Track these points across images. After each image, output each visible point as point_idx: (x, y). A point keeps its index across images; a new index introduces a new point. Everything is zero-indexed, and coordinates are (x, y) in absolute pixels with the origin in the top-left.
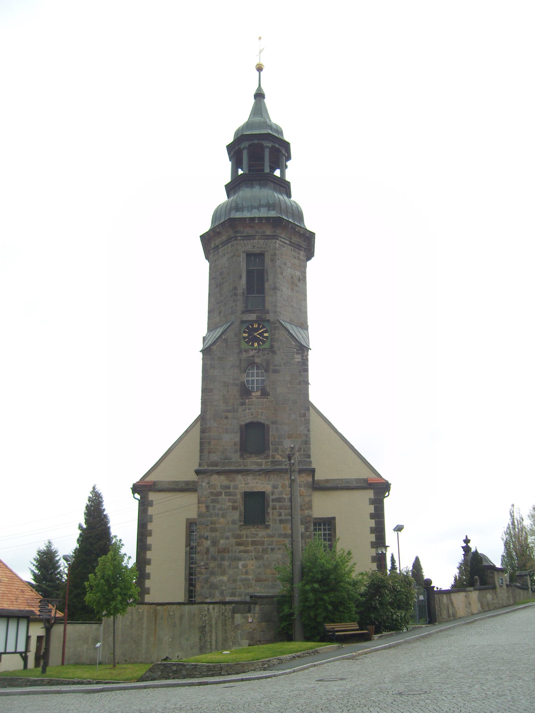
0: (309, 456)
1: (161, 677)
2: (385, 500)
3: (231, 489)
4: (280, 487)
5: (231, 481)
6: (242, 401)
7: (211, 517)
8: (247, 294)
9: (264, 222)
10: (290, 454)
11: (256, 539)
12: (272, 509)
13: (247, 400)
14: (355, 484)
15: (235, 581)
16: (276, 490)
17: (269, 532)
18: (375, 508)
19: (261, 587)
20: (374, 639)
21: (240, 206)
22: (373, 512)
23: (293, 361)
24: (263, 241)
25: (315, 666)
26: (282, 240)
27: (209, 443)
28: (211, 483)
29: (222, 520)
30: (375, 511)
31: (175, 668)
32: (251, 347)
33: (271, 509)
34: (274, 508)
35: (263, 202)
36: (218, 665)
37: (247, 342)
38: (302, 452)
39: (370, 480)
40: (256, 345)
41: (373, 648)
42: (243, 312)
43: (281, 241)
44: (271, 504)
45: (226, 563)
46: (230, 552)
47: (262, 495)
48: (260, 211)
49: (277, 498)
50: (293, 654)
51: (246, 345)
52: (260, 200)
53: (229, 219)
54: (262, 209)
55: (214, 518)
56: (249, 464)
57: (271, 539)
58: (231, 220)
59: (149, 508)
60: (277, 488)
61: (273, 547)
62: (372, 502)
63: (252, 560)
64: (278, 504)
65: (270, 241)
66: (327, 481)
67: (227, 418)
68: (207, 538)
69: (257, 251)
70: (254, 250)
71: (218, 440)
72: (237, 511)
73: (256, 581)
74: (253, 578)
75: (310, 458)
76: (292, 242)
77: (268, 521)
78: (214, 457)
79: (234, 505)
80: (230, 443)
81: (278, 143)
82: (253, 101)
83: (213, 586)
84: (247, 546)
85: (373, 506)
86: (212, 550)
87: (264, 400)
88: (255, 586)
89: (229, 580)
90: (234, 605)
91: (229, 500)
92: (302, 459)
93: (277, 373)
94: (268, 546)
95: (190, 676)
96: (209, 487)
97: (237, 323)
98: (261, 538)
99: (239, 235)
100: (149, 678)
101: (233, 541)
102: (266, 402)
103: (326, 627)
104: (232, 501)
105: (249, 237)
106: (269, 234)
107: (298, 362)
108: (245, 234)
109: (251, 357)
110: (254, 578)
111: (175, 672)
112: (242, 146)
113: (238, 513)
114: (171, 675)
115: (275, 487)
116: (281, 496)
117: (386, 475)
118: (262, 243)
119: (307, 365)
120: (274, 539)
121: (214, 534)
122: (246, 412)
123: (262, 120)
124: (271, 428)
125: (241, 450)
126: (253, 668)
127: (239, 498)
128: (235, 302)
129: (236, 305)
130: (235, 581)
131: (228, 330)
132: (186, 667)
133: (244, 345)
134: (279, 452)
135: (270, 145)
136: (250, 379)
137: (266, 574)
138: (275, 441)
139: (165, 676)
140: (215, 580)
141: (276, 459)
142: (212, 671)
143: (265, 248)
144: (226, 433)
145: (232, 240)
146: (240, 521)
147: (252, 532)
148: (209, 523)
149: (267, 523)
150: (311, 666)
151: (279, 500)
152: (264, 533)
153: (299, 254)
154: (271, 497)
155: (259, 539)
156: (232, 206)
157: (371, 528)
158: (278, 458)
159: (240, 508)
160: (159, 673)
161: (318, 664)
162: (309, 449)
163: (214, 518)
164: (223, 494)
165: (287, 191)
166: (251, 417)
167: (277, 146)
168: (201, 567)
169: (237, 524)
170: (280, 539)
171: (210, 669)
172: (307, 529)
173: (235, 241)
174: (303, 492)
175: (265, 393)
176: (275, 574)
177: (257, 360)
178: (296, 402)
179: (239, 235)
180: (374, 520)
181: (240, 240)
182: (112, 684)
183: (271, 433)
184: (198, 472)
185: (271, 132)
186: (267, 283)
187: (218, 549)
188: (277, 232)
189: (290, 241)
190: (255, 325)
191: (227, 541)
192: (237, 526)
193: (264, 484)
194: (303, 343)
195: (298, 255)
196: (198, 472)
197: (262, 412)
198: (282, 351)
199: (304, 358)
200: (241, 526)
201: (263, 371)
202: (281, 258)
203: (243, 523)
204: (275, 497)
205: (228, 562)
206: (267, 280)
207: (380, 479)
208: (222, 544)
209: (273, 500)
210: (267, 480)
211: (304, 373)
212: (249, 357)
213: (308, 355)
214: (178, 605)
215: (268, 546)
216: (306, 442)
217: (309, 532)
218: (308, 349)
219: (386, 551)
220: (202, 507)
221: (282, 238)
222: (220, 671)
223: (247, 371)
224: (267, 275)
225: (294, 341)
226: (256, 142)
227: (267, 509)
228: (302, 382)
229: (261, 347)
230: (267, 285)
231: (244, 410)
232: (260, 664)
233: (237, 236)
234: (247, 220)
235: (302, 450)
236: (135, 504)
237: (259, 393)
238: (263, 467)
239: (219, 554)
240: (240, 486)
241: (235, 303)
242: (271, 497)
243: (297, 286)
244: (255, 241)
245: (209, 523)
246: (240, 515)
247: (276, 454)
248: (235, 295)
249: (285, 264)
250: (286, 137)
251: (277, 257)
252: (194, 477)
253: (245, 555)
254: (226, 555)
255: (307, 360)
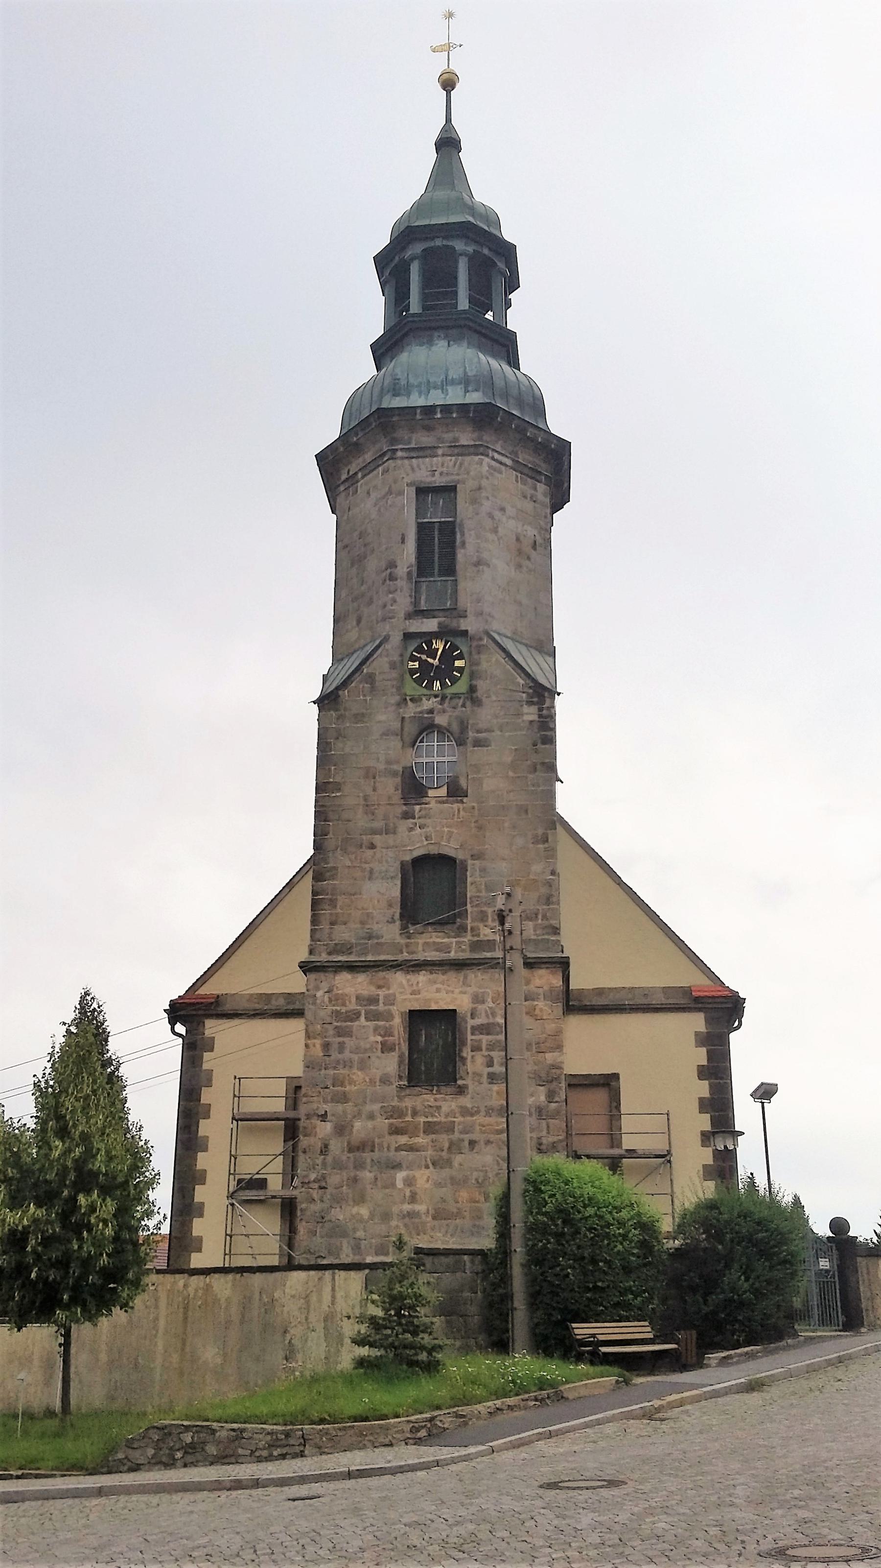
0: (556, 931)
1: (153, 1461)
2: (733, 1036)
3: (381, 1005)
4: (489, 1000)
5: (379, 987)
6: (404, 808)
7: (335, 1068)
8: (418, 576)
9: (454, 415)
10: (502, 910)
11: (435, 1119)
12: (472, 1051)
13: (417, 808)
14: (659, 999)
15: (386, 1217)
16: (480, 1007)
17: (466, 1101)
18: (710, 1056)
19: (447, 1232)
20: (708, 1366)
21: (403, 382)
22: (705, 1063)
23: (520, 720)
24: (453, 458)
25: (550, 1435)
26: (496, 456)
27: (333, 903)
28: (335, 991)
29: (358, 1075)
30: (708, 1061)
31: (188, 1438)
32: (425, 692)
33: (469, 1050)
34: (476, 1048)
35: (454, 374)
36: (298, 1430)
37: (419, 681)
38: (540, 921)
39: (695, 991)
40: (437, 685)
41: (705, 1389)
42: (409, 616)
43: (493, 458)
44: (470, 1037)
45: (367, 1175)
46: (376, 1149)
47: (449, 1016)
48: (447, 394)
49: (482, 1025)
50: (495, 1402)
51: (414, 684)
52: (447, 370)
53: (378, 409)
54: (450, 389)
55: (342, 1071)
56: (420, 948)
57: (469, 1118)
58: (381, 412)
59: (205, 1054)
60: (483, 1002)
61: (473, 1137)
62: (703, 1040)
63: (427, 1167)
64: (485, 1039)
65: (468, 459)
66: (600, 992)
67: (372, 846)
68: (324, 1117)
69: (439, 481)
70: (433, 479)
71: (351, 894)
72: (393, 1053)
73: (434, 1218)
74: (428, 1210)
75: (559, 934)
76: (518, 462)
77: (462, 1078)
78: (343, 934)
79: (386, 1041)
80: (378, 901)
81: (487, 246)
82: (432, 156)
83: (338, 1231)
84: (414, 1135)
85: (704, 1050)
86: (336, 1147)
87: (455, 806)
88: (433, 1229)
89: (372, 1216)
90: (367, 1271)
91: (376, 1029)
92: (540, 938)
93: (484, 746)
94: (462, 1136)
95: (223, 1461)
96: (330, 1000)
97: (396, 638)
98: (447, 1116)
99: (401, 446)
100: (124, 1465)
101: (383, 1123)
102: (459, 810)
103: (577, 1331)
104: (382, 1033)
105: (422, 451)
106: (466, 443)
107: (531, 722)
108: (413, 446)
109: (428, 713)
110: (431, 1212)
111: (190, 1449)
112: (408, 254)
113: (396, 1059)
114: (179, 1455)
115: (478, 999)
116: (491, 1020)
117: (732, 982)
118: (451, 464)
119: (554, 730)
120: (480, 1119)
121: (340, 1108)
122: (413, 833)
123: (453, 194)
124: (469, 868)
125: (402, 916)
126: (387, 1441)
127: (398, 1023)
128: (391, 593)
129: (394, 601)
130: (386, 1217)
131: (375, 656)
132: (218, 1434)
133: (411, 688)
134: (487, 921)
135: (470, 249)
136: (425, 760)
137: (457, 1202)
138: (478, 897)
139: (164, 1459)
140: (339, 1215)
141: (482, 937)
142: (279, 1446)
143: (458, 474)
144: (370, 879)
145: (385, 459)
146: (400, 1077)
147: (426, 1103)
148: (329, 1083)
149: (460, 1082)
150: (540, 1437)
151: (485, 1029)
152: (453, 1105)
153: (535, 489)
154: (471, 1023)
155: (443, 1119)
156: (385, 384)
157: (701, 1100)
158: (485, 935)
159: (399, 1048)
160: (151, 1452)
161: (559, 1430)
162: (556, 914)
163: (342, 1071)
164: (362, 1018)
165: (508, 351)
166: (426, 843)
167: (486, 251)
168: (311, 1185)
169: (391, 1084)
170: (491, 1119)
171: (277, 1439)
172: (551, 1096)
173: (390, 461)
174: (541, 1010)
175: (456, 792)
176: (478, 1202)
177: (441, 720)
178: (526, 812)
179: (401, 446)
180: (706, 1082)
181: (402, 458)
182: (34, 1481)
183: (469, 880)
184: (306, 967)
185: (471, 219)
186: (462, 551)
187: (349, 1143)
188: (485, 438)
189: (513, 460)
190: (434, 642)
191: (370, 1124)
192: (392, 1090)
193: (453, 992)
194: (542, 680)
195: (533, 492)
196: (306, 967)
197: (450, 834)
198: (494, 698)
199: (545, 712)
200: (400, 1087)
201: (454, 743)
202: (493, 496)
203: (406, 1083)
204: (477, 1021)
205: (370, 1172)
206: (463, 544)
207: (720, 988)
208: (358, 1130)
209: (475, 1029)
210: (461, 983)
211: (543, 746)
212: (421, 712)
213: (553, 707)
214: (238, 1273)
215: (462, 1136)
216: (548, 899)
217: (556, 1102)
218: (553, 693)
219: (735, 1144)
220: (314, 1046)
221: (497, 452)
222: (302, 1448)
223: (417, 744)
224: (463, 534)
225: (522, 675)
226: (438, 242)
227: (461, 1050)
228: (538, 767)
229: (449, 691)
230: (461, 556)
231: (411, 829)
232: (407, 1428)
233: (397, 450)
234: (418, 411)
235: (540, 917)
236: (176, 1047)
237: (443, 792)
238: (452, 955)
239: (351, 1155)
240: (399, 998)
241: (391, 596)
242: (471, 1023)
243: (529, 558)
244: (435, 459)
245: (329, 1083)
246: (400, 1063)
247: (481, 925)
248: (392, 578)
249: (503, 509)
250: (508, 234)
251: (484, 494)
252: (297, 983)
253: (411, 1156)
254: (367, 1156)
255: (552, 717)
